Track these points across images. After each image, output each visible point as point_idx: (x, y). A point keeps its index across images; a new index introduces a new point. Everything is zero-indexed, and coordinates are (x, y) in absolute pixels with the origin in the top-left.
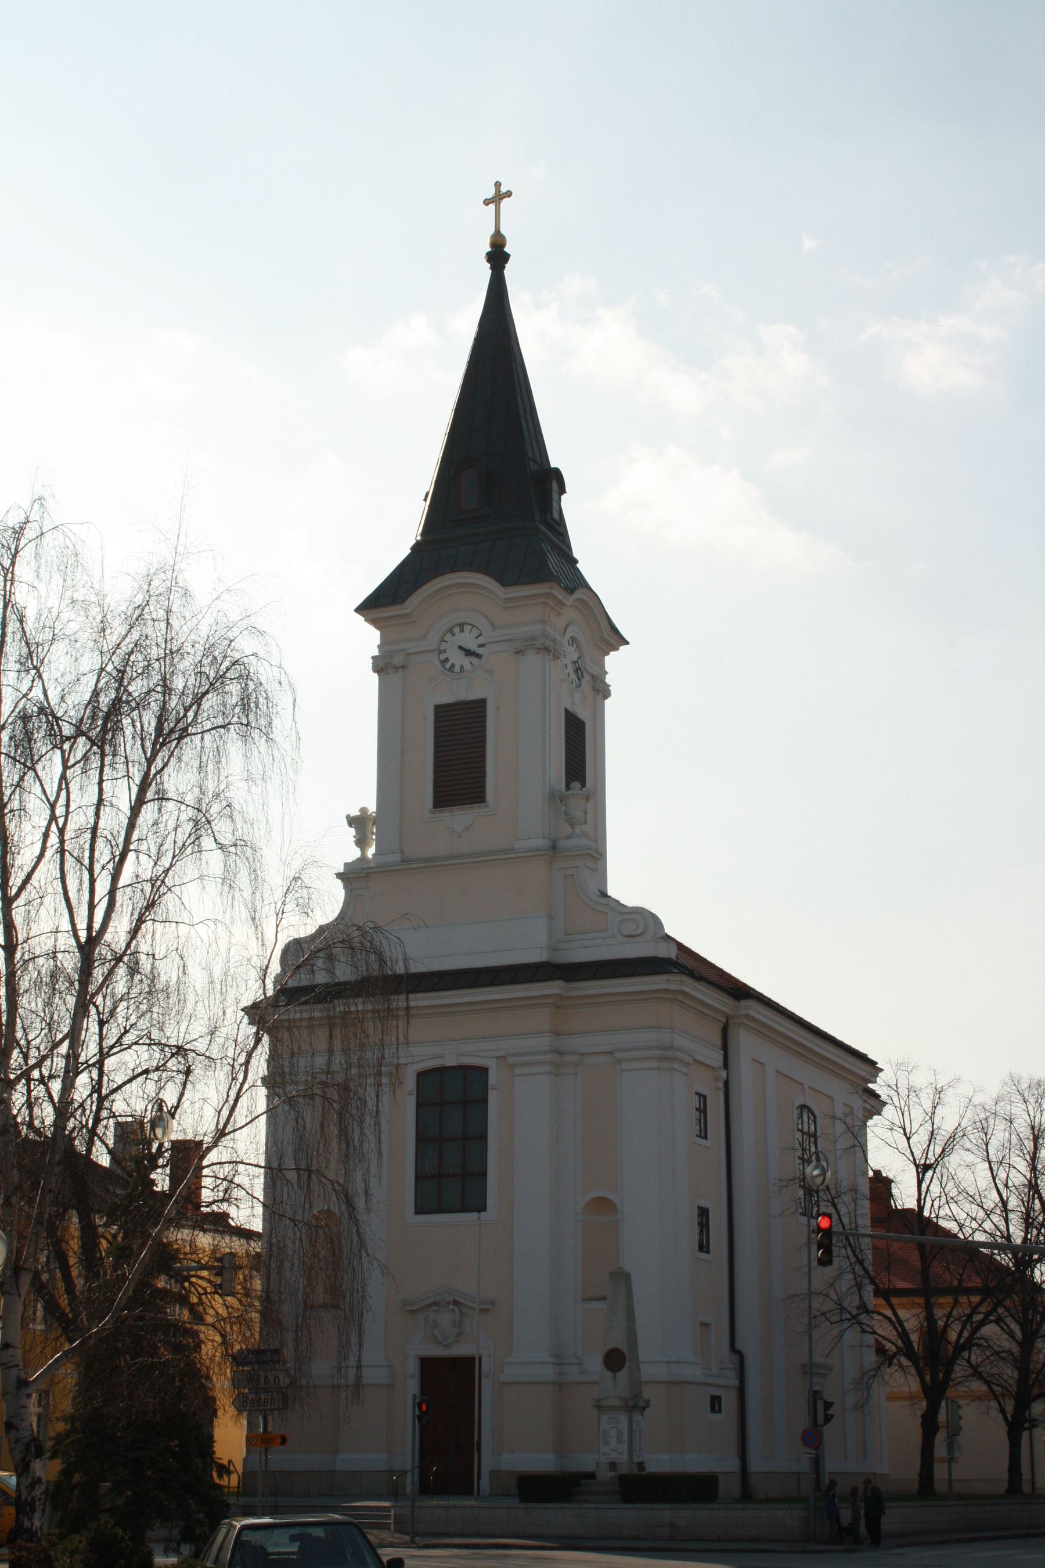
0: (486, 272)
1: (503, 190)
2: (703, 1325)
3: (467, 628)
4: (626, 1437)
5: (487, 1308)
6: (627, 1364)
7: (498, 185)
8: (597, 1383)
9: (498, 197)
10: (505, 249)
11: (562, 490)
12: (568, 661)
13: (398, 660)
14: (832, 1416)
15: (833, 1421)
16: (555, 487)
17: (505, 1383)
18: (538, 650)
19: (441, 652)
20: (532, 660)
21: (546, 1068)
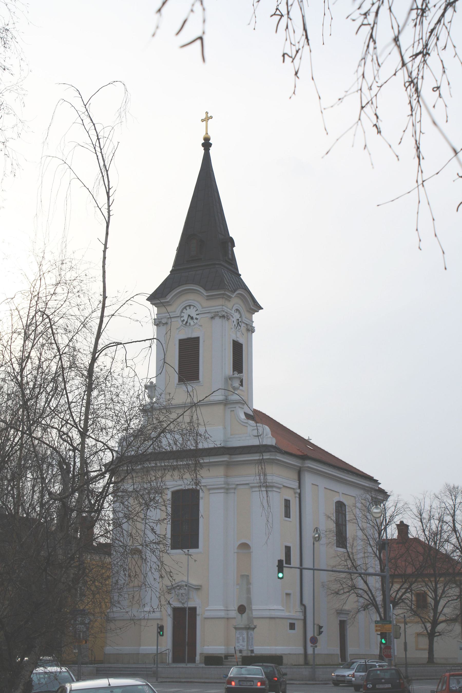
0: (201, 151)
1: (209, 115)
2: (288, 595)
3: (192, 307)
4: (246, 640)
5: (198, 588)
6: (247, 610)
7: (207, 113)
8: (235, 618)
9: (207, 118)
10: (210, 142)
11: (233, 245)
12: (235, 319)
13: (164, 321)
14: (322, 632)
15: (322, 634)
16: (230, 244)
17: (205, 618)
18: (220, 317)
19: (181, 317)
20: (218, 321)
21: (222, 491)
